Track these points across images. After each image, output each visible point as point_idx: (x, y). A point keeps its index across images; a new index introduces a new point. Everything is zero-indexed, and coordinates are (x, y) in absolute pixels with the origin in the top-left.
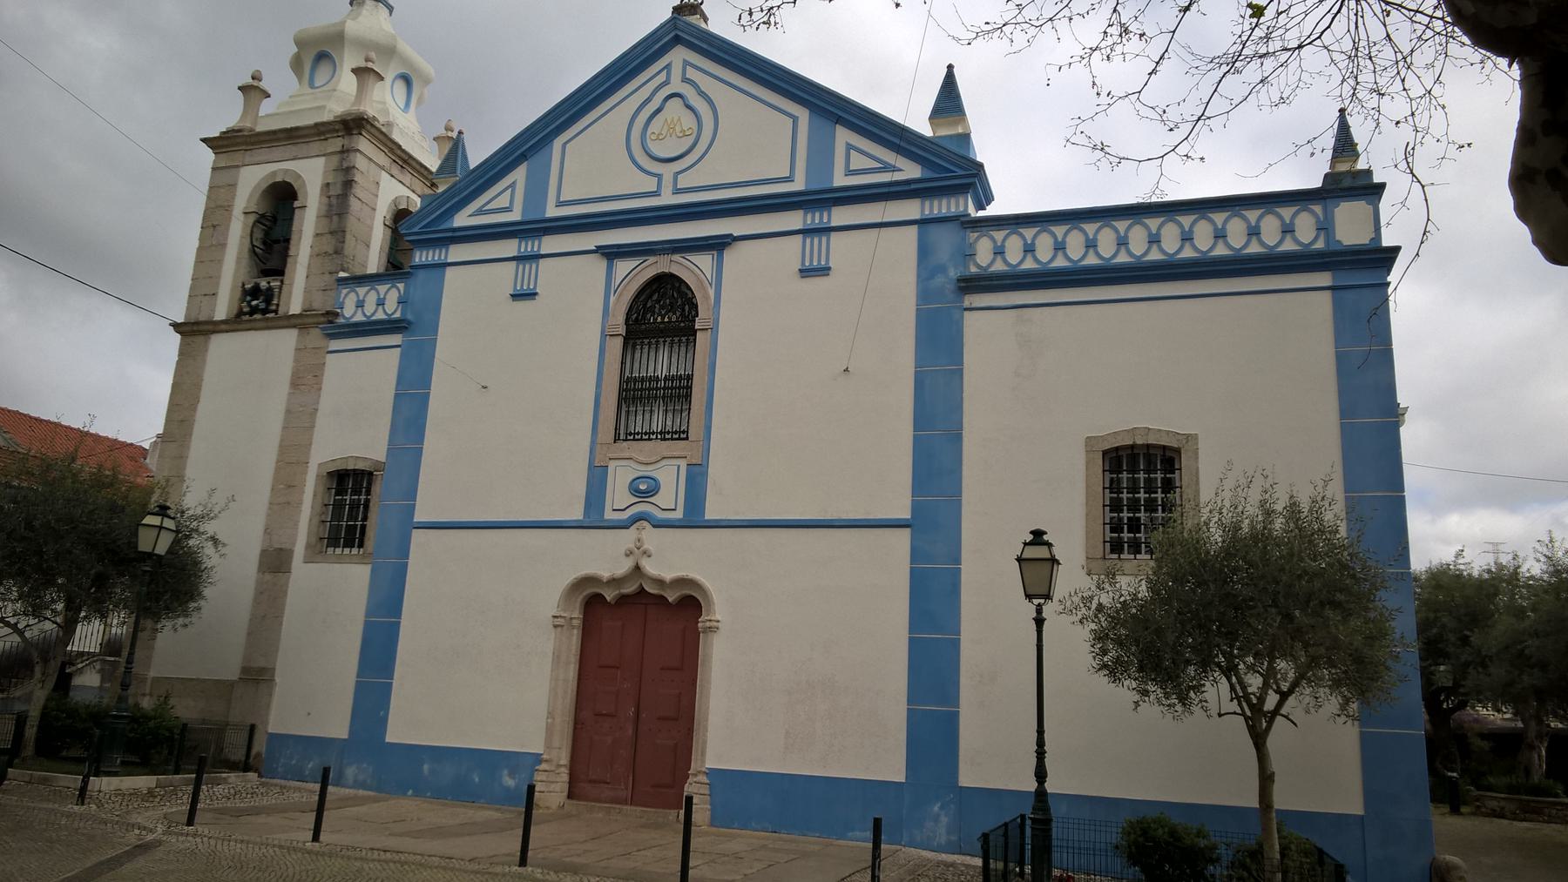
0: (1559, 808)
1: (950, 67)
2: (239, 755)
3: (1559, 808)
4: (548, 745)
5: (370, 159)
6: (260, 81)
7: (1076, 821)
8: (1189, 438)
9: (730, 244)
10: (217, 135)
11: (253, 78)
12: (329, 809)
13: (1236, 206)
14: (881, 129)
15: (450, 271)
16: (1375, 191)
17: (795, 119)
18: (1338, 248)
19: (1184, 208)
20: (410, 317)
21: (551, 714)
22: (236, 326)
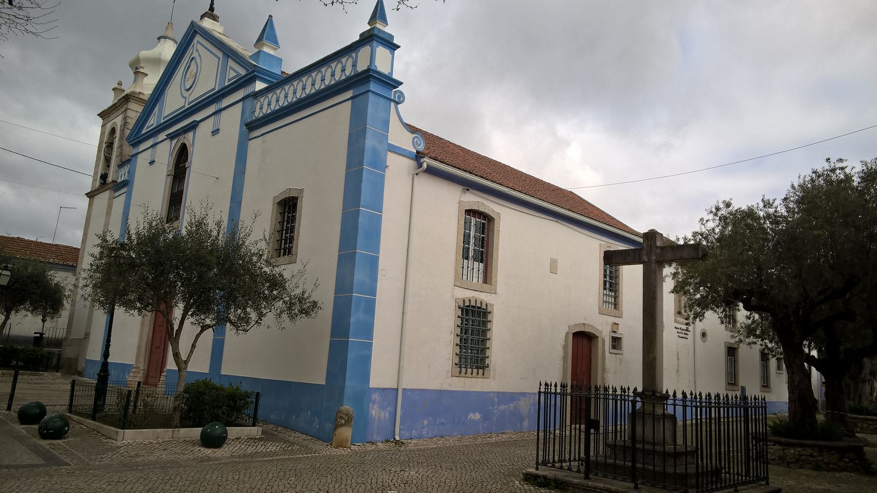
0: (870, 423)
1: (270, 16)
2: (693, 408)
3: (870, 423)
4: (137, 361)
5: (137, 111)
6: (121, 85)
7: (123, 383)
8: (302, 190)
9: (198, 125)
10: (358, 38)
11: (118, 84)
12: (20, 383)
13: (329, 62)
14: (271, 46)
15: (139, 156)
16: (371, 39)
17: (219, 59)
18: (375, 69)
19: (313, 68)
20: (129, 179)
21: (139, 348)
22: (102, 190)
